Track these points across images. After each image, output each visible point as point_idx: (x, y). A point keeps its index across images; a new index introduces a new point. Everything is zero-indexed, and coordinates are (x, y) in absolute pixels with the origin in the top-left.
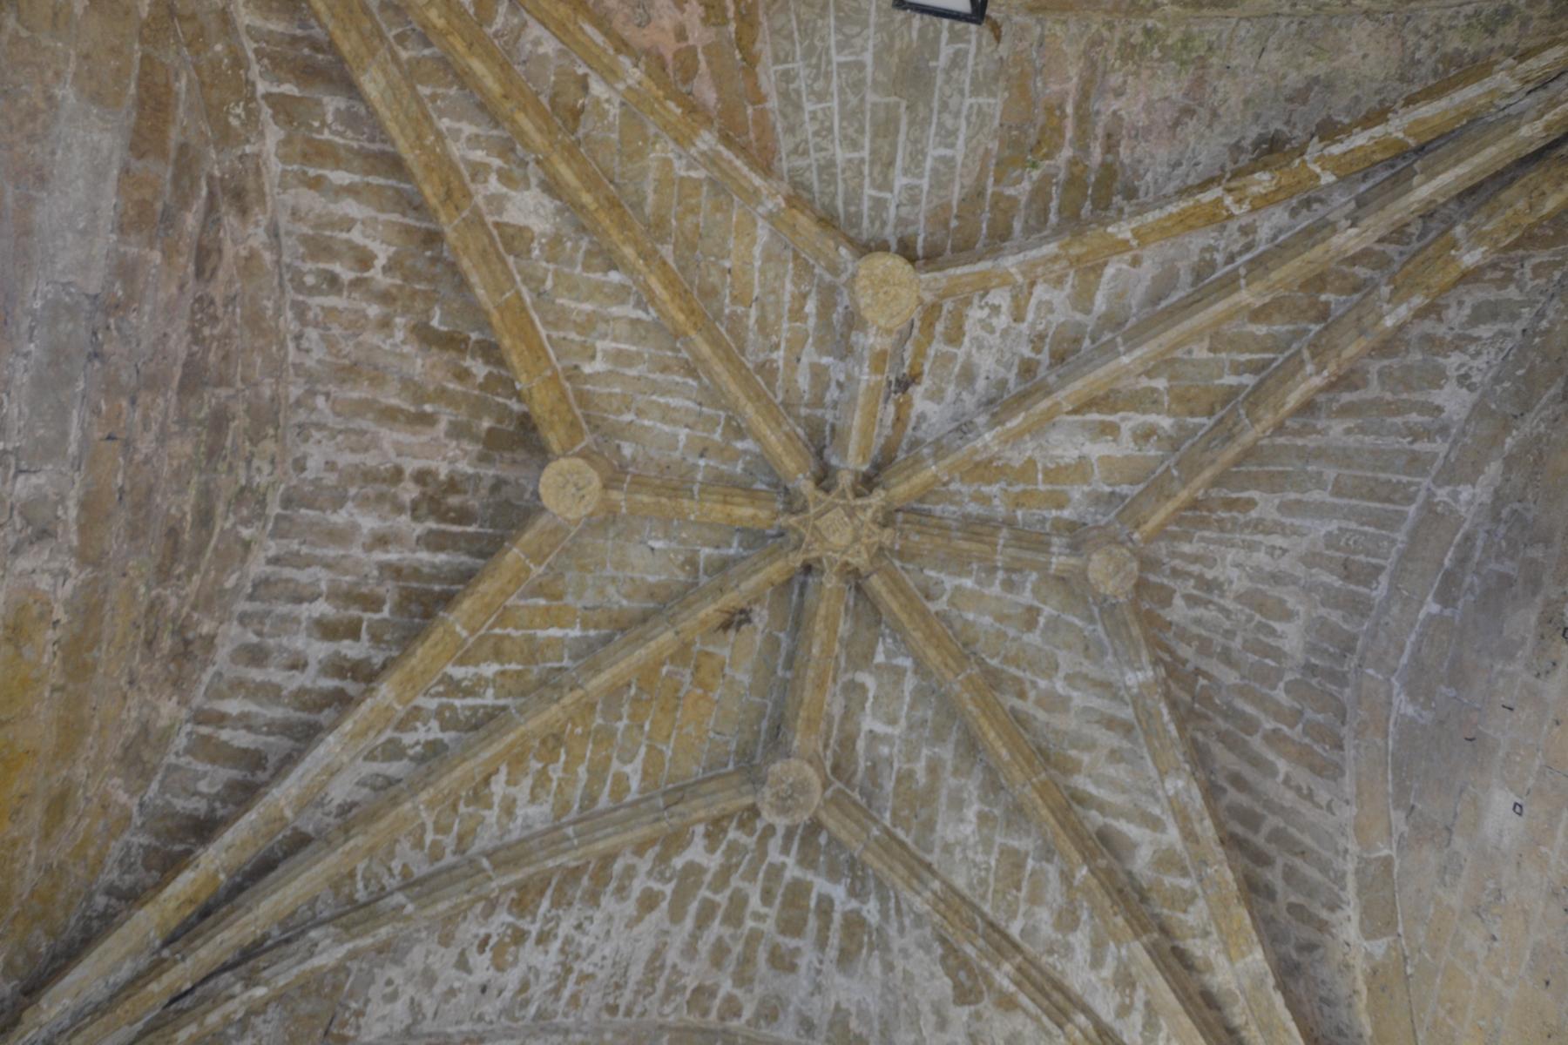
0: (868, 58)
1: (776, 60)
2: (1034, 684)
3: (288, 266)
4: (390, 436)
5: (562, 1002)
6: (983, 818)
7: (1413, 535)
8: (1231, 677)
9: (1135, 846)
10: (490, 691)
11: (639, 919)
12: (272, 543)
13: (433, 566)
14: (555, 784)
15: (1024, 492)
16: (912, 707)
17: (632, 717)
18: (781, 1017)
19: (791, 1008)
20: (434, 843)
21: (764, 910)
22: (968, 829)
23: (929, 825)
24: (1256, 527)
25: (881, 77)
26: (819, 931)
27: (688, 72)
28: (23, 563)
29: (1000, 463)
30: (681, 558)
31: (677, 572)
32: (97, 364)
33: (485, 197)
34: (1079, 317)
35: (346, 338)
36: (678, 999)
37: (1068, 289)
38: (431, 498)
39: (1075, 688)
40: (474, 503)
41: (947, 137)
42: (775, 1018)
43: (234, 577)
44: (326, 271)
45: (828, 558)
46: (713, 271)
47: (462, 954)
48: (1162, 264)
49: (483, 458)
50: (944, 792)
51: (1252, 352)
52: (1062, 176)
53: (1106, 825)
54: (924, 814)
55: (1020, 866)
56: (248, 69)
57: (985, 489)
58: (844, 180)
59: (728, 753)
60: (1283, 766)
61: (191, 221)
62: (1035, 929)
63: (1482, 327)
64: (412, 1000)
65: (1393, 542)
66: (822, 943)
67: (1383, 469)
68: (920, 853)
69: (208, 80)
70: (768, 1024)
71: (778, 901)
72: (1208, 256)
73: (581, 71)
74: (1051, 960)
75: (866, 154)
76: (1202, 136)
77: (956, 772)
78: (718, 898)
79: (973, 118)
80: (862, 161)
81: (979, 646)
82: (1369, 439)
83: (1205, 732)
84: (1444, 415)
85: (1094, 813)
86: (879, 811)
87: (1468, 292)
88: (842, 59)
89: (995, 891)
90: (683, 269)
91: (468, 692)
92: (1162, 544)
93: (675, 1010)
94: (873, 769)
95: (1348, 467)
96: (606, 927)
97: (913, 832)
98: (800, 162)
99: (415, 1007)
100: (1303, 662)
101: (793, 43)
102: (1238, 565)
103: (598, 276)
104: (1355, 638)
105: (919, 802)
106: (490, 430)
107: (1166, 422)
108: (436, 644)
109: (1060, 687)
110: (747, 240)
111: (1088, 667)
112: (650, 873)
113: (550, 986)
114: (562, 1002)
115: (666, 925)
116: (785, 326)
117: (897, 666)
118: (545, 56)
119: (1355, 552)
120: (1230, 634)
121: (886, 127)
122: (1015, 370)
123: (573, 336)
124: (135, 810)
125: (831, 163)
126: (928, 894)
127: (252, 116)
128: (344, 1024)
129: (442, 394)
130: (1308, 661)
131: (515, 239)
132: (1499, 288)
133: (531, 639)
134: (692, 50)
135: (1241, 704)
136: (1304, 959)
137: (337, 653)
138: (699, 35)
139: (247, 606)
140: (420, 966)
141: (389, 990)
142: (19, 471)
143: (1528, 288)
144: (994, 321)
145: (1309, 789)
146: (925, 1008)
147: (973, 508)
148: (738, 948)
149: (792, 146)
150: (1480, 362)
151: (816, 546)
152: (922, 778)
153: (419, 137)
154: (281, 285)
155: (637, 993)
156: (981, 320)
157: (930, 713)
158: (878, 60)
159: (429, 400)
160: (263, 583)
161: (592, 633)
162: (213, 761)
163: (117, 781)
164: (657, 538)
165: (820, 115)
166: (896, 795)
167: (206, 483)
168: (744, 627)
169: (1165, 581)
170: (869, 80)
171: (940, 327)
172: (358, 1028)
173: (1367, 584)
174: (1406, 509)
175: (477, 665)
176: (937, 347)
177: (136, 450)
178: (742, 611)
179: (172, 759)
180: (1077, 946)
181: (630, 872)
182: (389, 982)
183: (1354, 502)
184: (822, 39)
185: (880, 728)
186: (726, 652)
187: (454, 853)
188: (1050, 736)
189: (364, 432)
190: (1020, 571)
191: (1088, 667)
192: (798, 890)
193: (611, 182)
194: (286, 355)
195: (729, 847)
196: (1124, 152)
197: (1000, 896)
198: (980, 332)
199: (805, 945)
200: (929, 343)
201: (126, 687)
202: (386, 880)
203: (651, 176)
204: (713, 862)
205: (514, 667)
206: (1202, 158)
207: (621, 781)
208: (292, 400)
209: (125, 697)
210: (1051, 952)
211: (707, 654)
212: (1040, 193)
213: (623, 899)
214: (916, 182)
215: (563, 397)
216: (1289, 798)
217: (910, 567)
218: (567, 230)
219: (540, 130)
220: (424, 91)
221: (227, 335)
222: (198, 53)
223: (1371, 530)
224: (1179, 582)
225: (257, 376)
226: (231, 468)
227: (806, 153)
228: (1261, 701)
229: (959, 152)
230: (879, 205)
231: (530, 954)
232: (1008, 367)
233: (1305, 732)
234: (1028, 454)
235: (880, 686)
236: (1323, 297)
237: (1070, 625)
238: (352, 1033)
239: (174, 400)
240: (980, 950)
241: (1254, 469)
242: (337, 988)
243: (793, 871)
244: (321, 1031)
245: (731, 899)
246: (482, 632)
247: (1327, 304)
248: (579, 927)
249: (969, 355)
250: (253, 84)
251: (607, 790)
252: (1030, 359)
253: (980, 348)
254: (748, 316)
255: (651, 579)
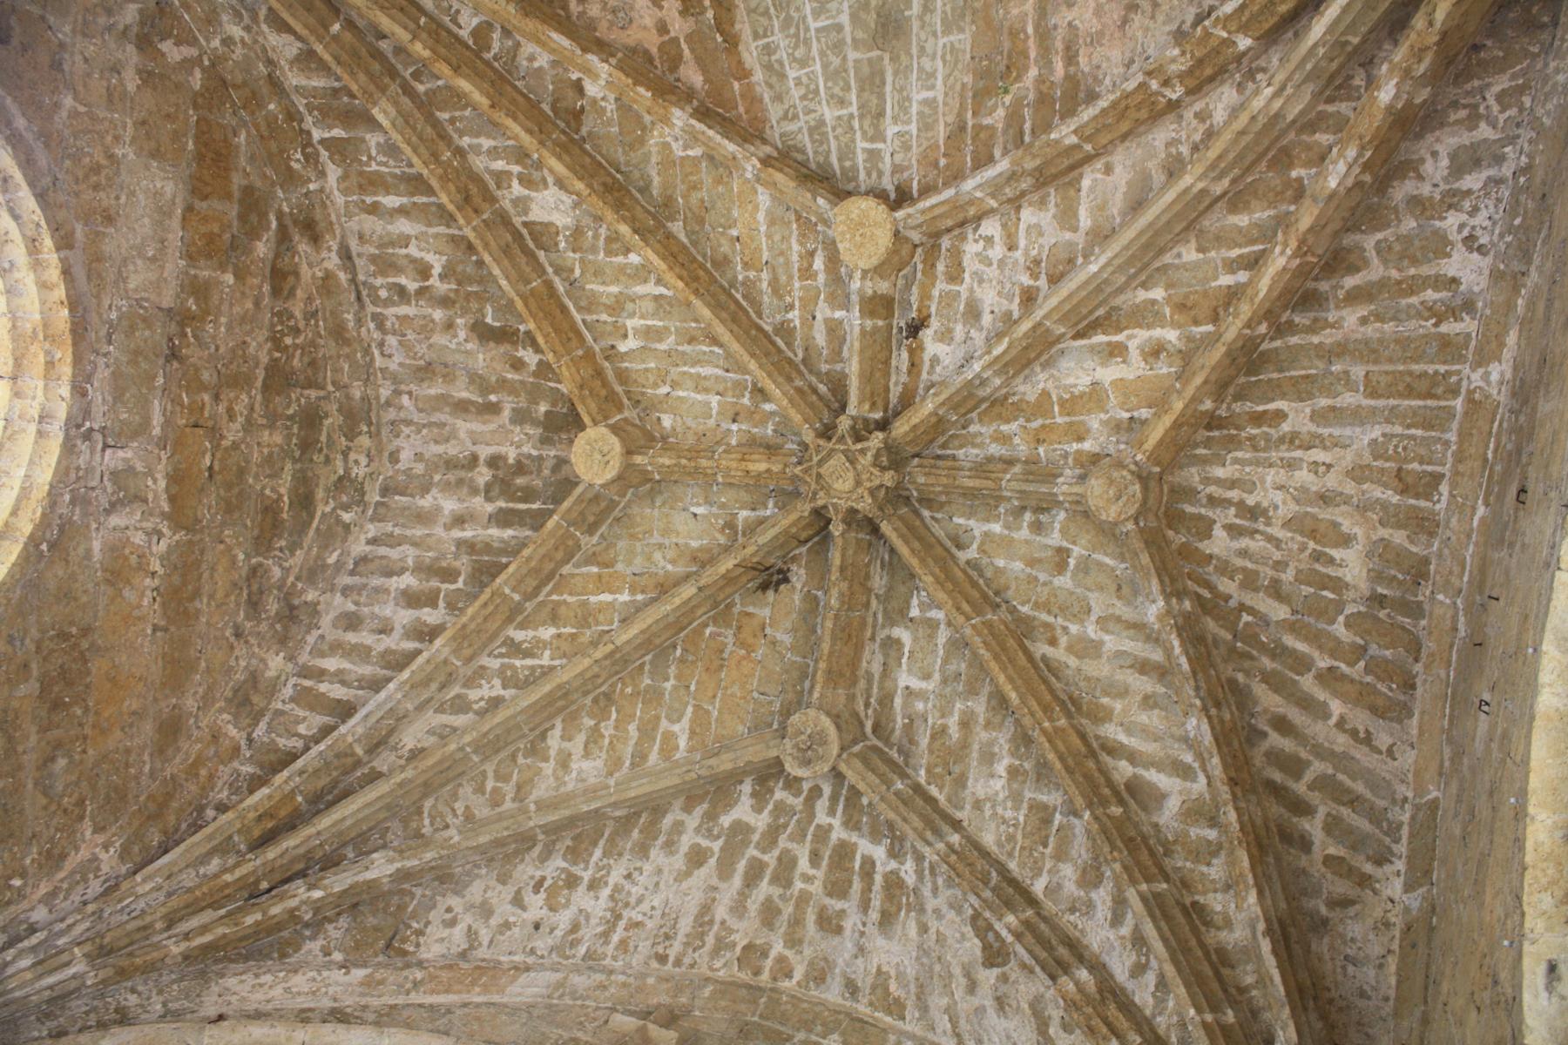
0: (845, 19)
1: (756, 36)
2: (1065, 629)
3: (364, 283)
4: (464, 426)
5: (612, 946)
6: (1013, 772)
7: (1463, 436)
8: (1280, 612)
9: (1162, 797)
10: (547, 653)
11: (688, 874)
12: (371, 526)
13: (502, 541)
14: (607, 741)
15: (1043, 426)
16: (945, 661)
17: (678, 677)
18: (829, 979)
19: (837, 971)
20: (495, 790)
21: (812, 872)
22: (998, 785)
23: (961, 782)
24: (1291, 442)
25: (860, 35)
26: (863, 892)
27: (675, 62)
28: (115, 520)
29: (1016, 398)
30: (721, 522)
31: (718, 535)
32: (176, 364)
33: (512, 201)
34: (1068, 235)
35: (420, 342)
36: (728, 955)
37: (1053, 210)
38: (502, 480)
39: (1107, 632)
40: (538, 483)
41: (928, 78)
42: (823, 980)
43: (335, 556)
44: (395, 284)
45: (834, 505)
46: (723, 241)
47: (518, 892)
48: (1133, 166)
49: (545, 441)
50: (976, 747)
51: (1240, 246)
52: (1031, 96)
53: (1135, 776)
54: (957, 769)
55: (1047, 821)
56: (302, 120)
57: (1004, 428)
58: (836, 138)
59: (772, 713)
60: (1336, 707)
61: (262, 248)
62: (1059, 886)
63: (1468, 177)
64: (470, 927)
65: (1447, 443)
66: (865, 906)
67: (1415, 359)
68: (950, 811)
69: (266, 134)
70: (818, 986)
71: (825, 863)
72: (1173, 150)
73: (574, 77)
74: (1072, 918)
75: (854, 109)
76: (1147, 29)
77: (988, 725)
78: (766, 858)
79: (948, 57)
80: (851, 116)
81: (1010, 593)
82: (1389, 327)
83: (1247, 673)
84: (1462, 288)
85: (1123, 764)
86: (916, 770)
87: (1438, 140)
88: (820, 24)
89: (1023, 848)
90: (695, 244)
91: (528, 654)
92: (1193, 470)
93: (725, 965)
94: (909, 728)
95: (1376, 362)
96: (656, 879)
97: (946, 790)
98: (791, 127)
99: (471, 933)
100: (1367, 594)
101: (770, 18)
102: (1281, 488)
103: (620, 259)
104: (1426, 561)
105: (951, 758)
106: (547, 413)
107: (1171, 335)
108: (486, 604)
109: (1092, 631)
110: (750, 207)
111: (1121, 609)
112: (697, 830)
113: (599, 929)
114: (612, 946)
115: (715, 881)
116: (797, 285)
117: (930, 619)
118: (540, 68)
119: (1406, 460)
120: (1280, 565)
121: (872, 81)
122: (1017, 300)
123: (604, 317)
124: (243, 743)
125: (821, 123)
126: (941, 846)
127: (311, 159)
128: (404, 940)
129: (503, 384)
130: (1373, 590)
131: (542, 234)
132: (1471, 129)
133: (585, 604)
134: (675, 40)
135: (1290, 641)
136: (1335, 915)
137: (418, 619)
138: (679, 27)
139: (348, 580)
140: (478, 899)
141: (448, 916)
142: (106, 446)
143: (1501, 124)
144: (990, 253)
145: (1367, 731)
146: (957, 971)
147: (995, 449)
148: (788, 910)
149: (781, 113)
150: (1481, 219)
151: (821, 494)
152: (954, 732)
153: (435, 156)
154: (359, 298)
155: (687, 944)
156: (977, 254)
157: (963, 665)
158: (854, 17)
159: (493, 391)
160: (363, 560)
161: (640, 597)
162: (312, 709)
163: (226, 716)
164: (699, 505)
165: (805, 80)
166: (931, 752)
167: (302, 471)
168: (782, 587)
169: (1203, 511)
170: (849, 40)
171: (940, 267)
172: (418, 945)
173: (1428, 497)
174: (1452, 403)
175: (536, 629)
176: (941, 286)
177: (222, 437)
178: (780, 571)
179: (280, 706)
180: (1099, 904)
181: (678, 827)
182: (449, 910)
183: (1392, 402)
184: (798, 9)
185: (916, 684)
186: (767, 612)
187: (514, 800)
188: (1082, 684)
189: (443, 425)
190: (1047, 510)
191: (1121, 609)
192: (844, 852)
193: (618, 171)
194: (372, 360)
195: (776, 807)
196: (1082, 60)
197: (1026, 853)
198: (978, 266)
199: (850, 905)
200: (933, 285)
201: (232, 639)
202: (450, 819)
203: (654, 160)
204: (761, 822)
205: (569, 630)
206: (1150, 52)
207: (669, 737)
208: (383, 400)
209: (232, 648)
210: (1072, 910)
211: (748, 614)
212: (1014, 117)
213: (672, 853)
214: (906, 128)
215: (599, 373)
216: (1341, 742)
217: (939, 516)
218: (587, 221)
219: (529, 132)
220: (444, 116)
221: (313, 344)
222: (253, 113)
223: (1419, 432)
224: (1218, 511)
225: (346, 379)
226: (328, 460)
227: (796, 117)
228: (1315, 638)
229: (939, 93)
230: (873, 155)
231: (581, 898)
232: (1010, 299)
233: (1367, 670)
234: (1041, 386)
235: (916, 639)
236: (1294, 174)
237: (1100, 564)
238: (412, 949)
239: (259, 397)
240: (984, 901)
241: (1275, 375)
242: (401, 908)
243: (838, 833)
244: (382, 943)
245: (779, 859)
246: (540, 598)
247: (1299, 180)
248: (628, 876)
249: (971, 290)
250: (309, 133)
251: (656, 747)
252: (1029, 287)
253: (981, 281)
254: (760, 280)
255: (694, 544)
